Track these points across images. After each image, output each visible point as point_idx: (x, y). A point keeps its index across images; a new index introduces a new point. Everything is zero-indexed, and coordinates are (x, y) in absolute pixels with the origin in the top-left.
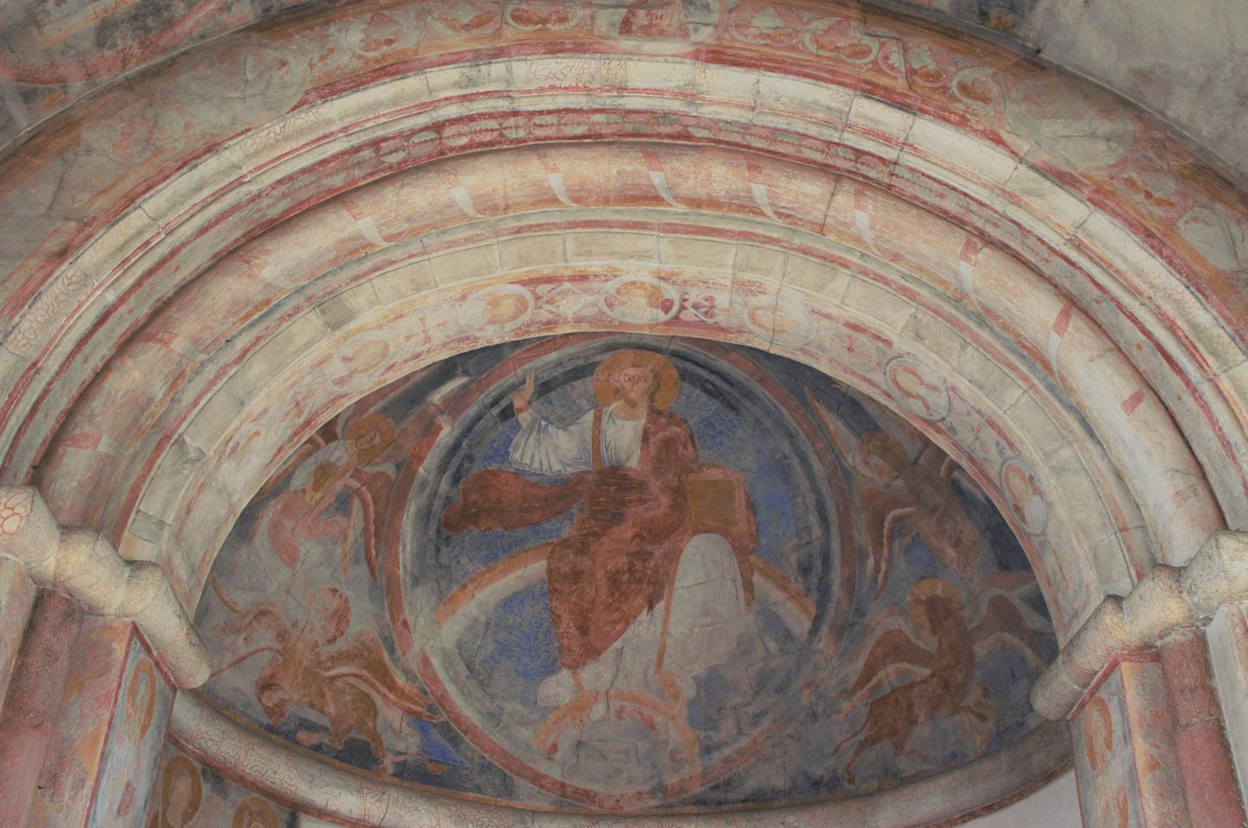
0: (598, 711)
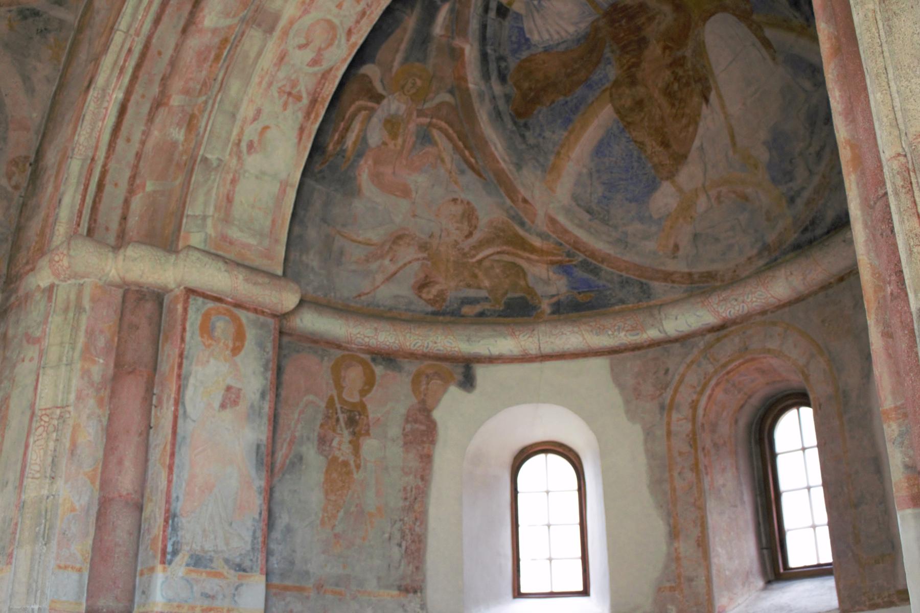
0: (702, 203)
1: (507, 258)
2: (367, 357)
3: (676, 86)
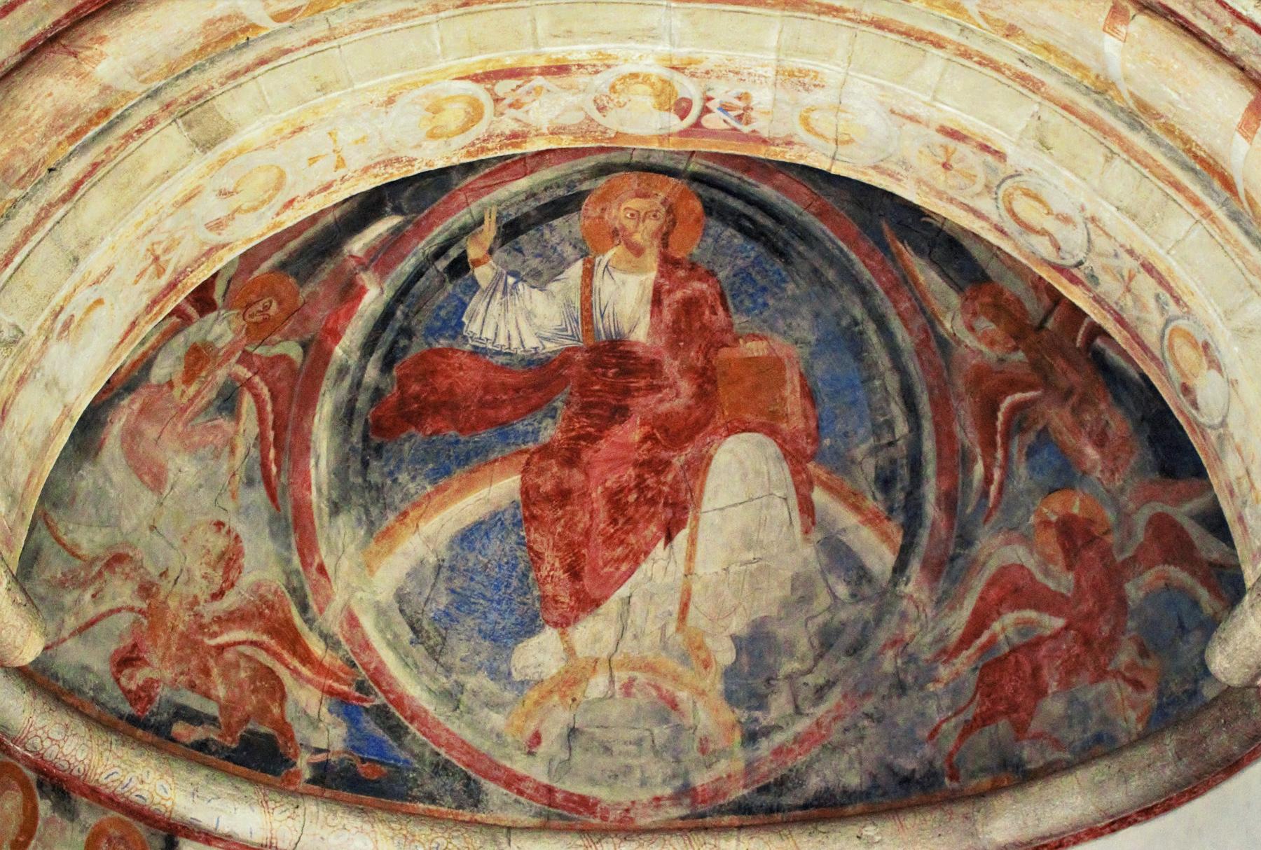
0: (597, 686)
1: (264, 658)
2: (31, 775)
3: (632, 497)
